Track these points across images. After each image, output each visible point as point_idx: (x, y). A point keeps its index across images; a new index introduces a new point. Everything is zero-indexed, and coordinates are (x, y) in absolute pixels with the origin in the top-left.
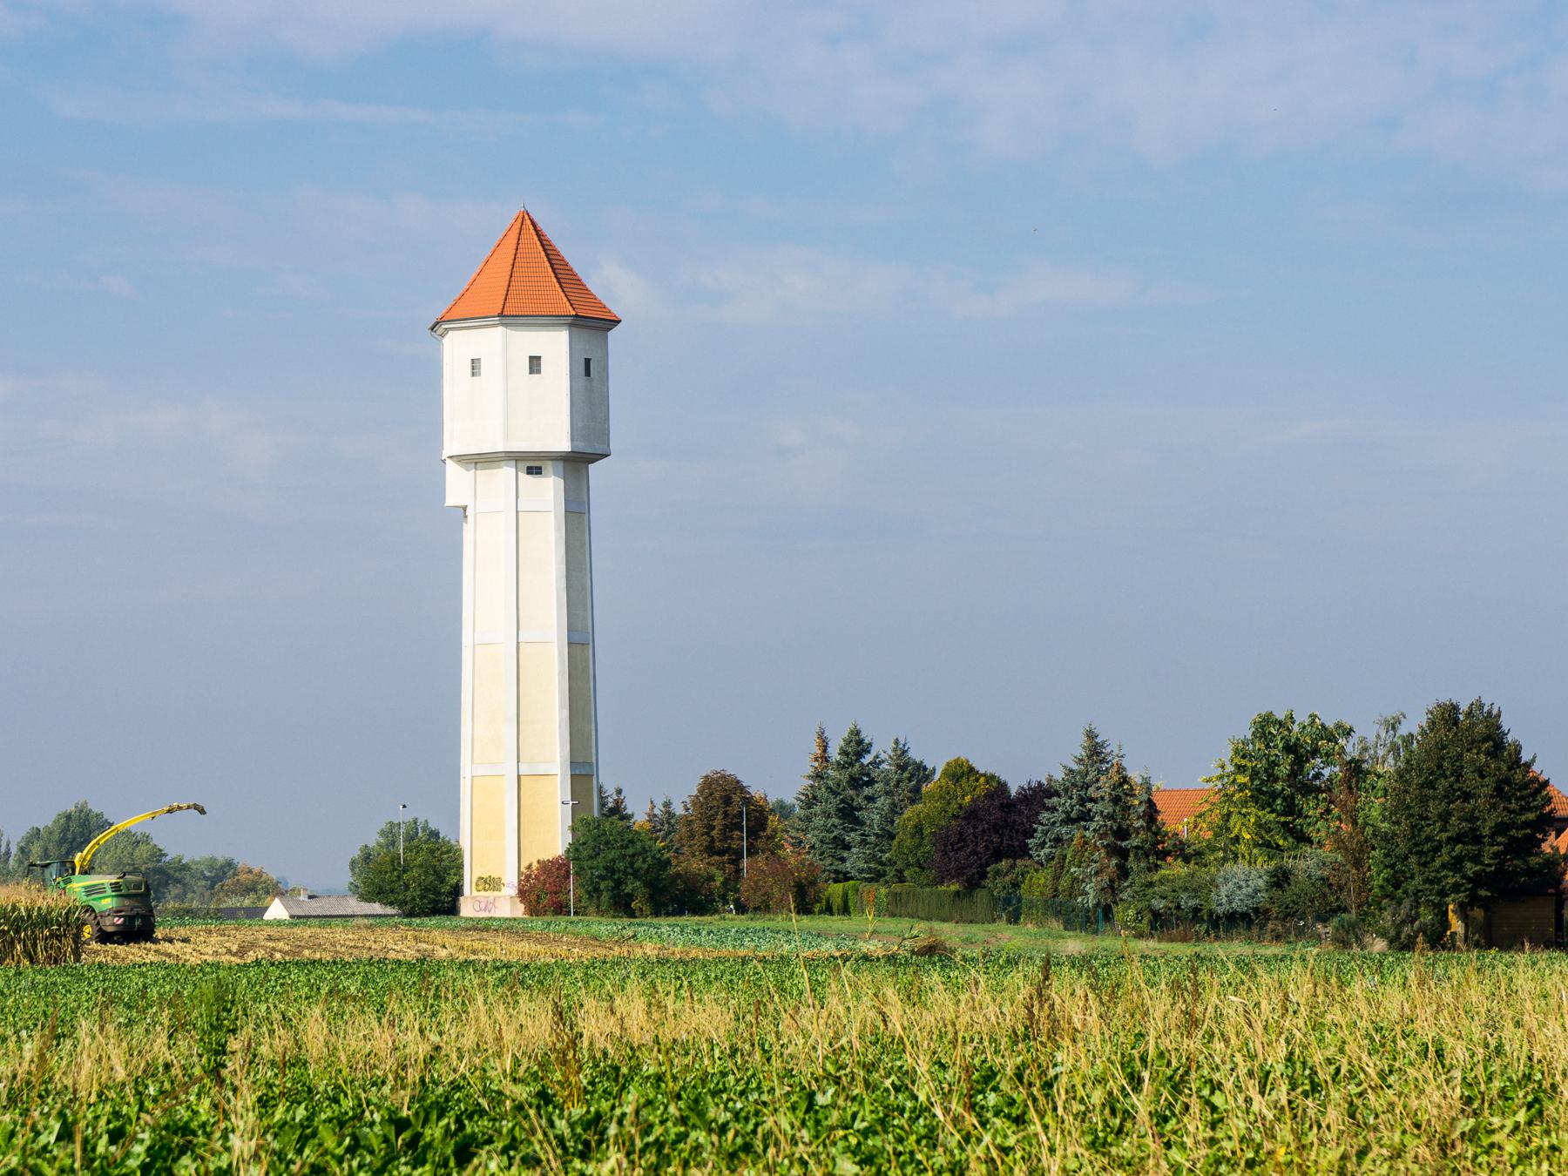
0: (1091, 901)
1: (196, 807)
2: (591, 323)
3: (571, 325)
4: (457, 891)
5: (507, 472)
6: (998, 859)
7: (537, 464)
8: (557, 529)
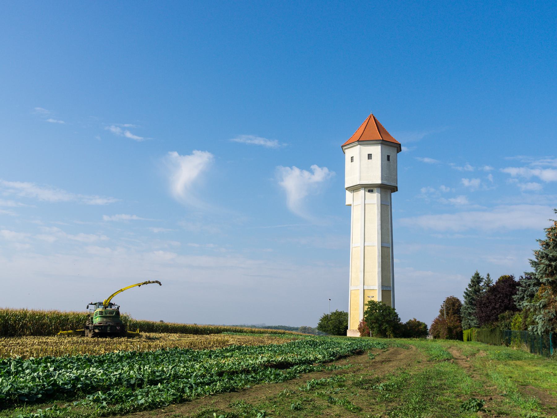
0: (540, 328)
1: (157, 282)
2: (391, 147)
3: (382, 144)
4: (347, 328)
6: (504, 311)
7: (372, 189)
8: (378, 209)
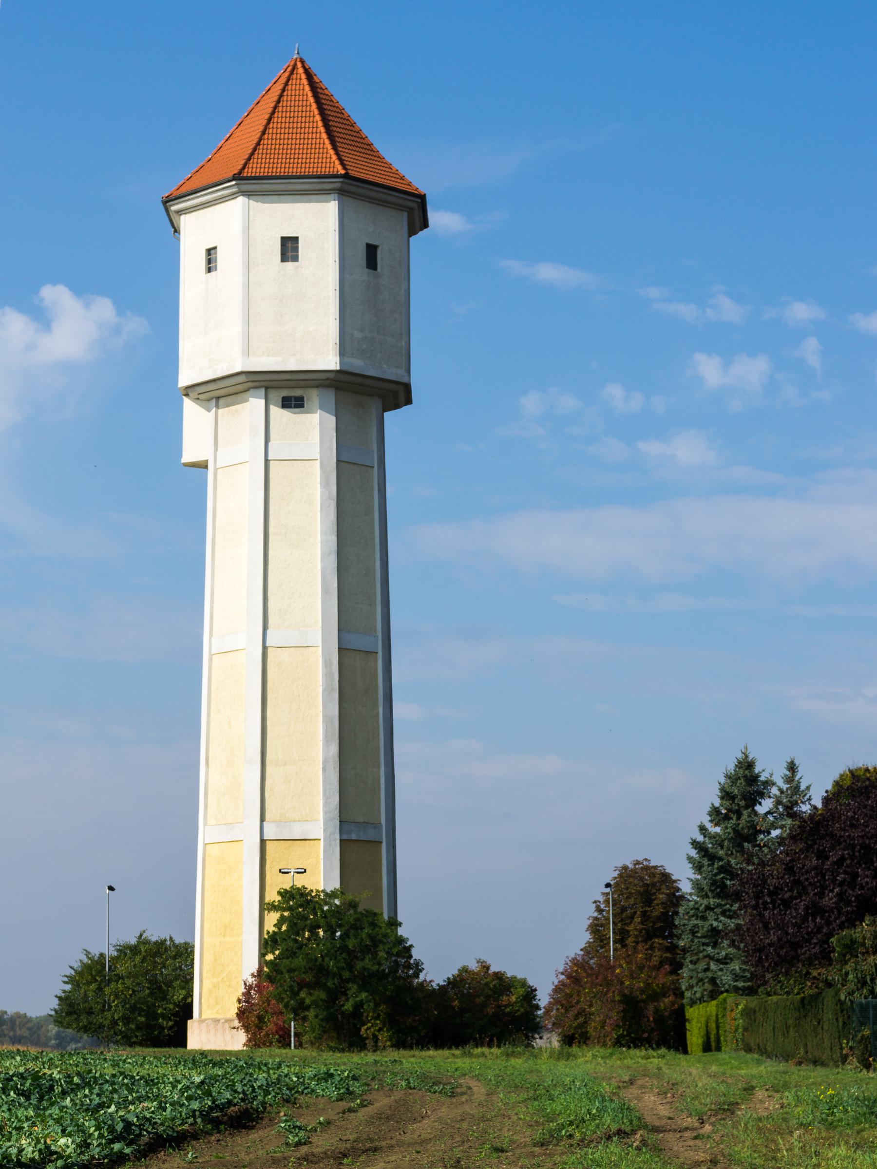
2: (386, 211)
4: (186, 1011)
5: (254, 406)
7: (297, 393)
8: (325, 484)
